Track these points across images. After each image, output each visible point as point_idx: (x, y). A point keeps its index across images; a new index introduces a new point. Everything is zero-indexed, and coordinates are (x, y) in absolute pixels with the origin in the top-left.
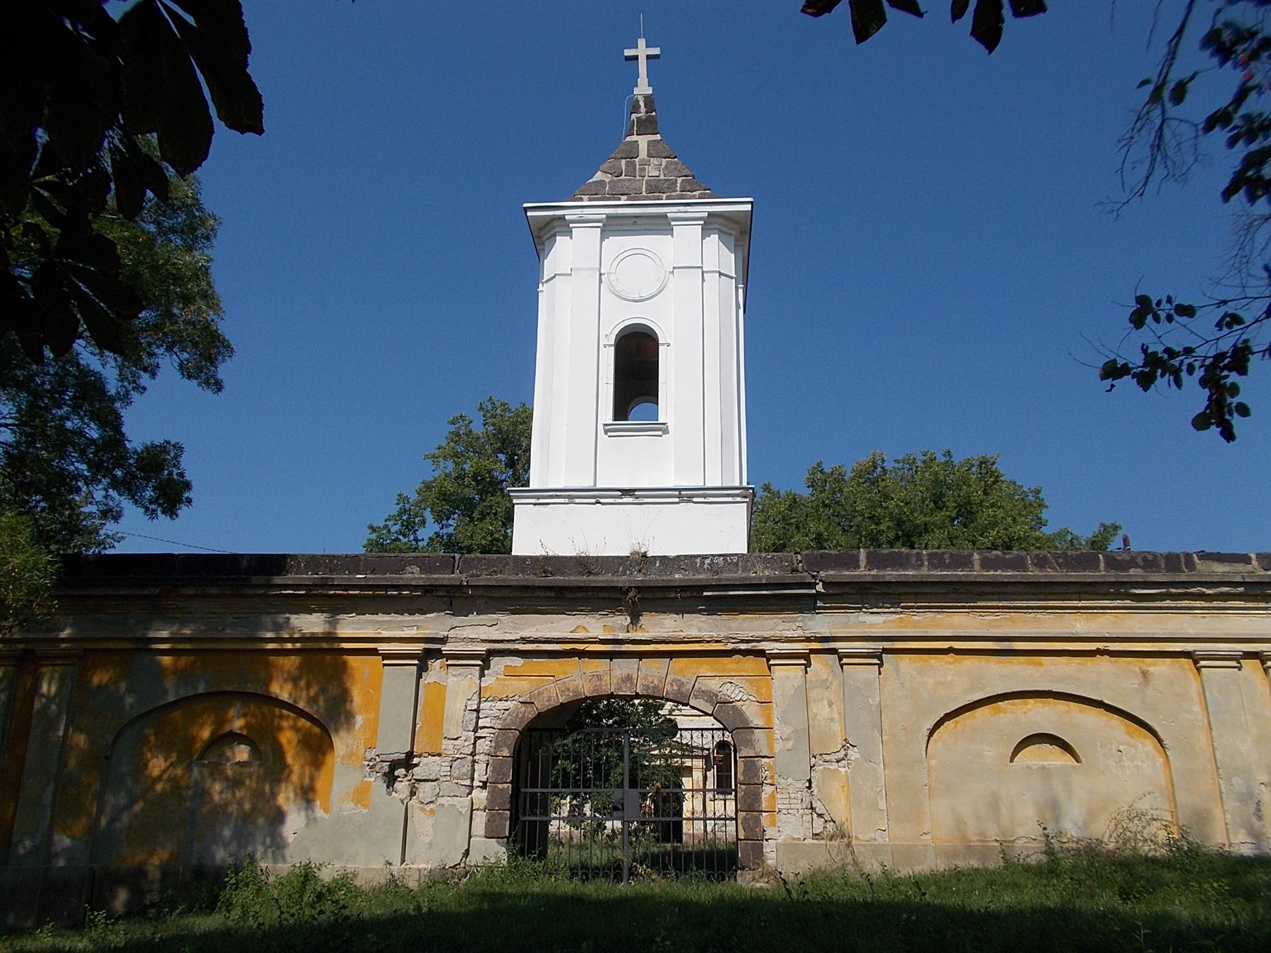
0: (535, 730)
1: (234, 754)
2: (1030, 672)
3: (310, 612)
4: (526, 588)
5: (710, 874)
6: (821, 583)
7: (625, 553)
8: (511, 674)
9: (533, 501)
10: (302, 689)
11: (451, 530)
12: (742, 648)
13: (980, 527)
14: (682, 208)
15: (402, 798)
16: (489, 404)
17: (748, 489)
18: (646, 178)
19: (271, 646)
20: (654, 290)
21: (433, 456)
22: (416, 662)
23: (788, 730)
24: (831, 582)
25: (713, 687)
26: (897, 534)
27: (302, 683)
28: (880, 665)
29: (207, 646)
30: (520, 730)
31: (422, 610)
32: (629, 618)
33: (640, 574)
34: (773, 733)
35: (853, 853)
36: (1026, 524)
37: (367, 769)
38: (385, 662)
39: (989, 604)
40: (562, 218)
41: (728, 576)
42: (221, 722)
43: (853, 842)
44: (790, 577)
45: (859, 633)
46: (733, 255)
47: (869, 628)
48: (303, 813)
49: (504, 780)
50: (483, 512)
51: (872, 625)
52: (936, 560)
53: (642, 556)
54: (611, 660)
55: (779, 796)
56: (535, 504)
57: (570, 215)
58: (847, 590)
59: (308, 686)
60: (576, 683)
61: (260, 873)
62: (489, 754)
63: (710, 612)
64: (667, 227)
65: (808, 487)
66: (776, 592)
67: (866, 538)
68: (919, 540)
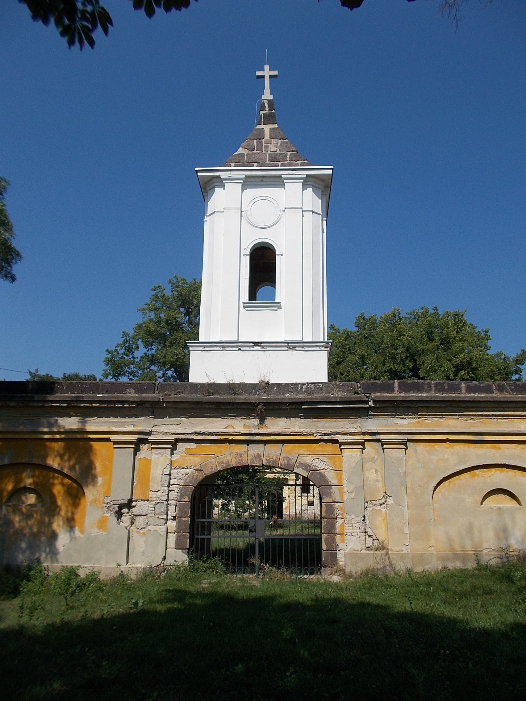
0: (204, 485)
1: (27, 499)
2: (493, 453)
3: (70, 416)
4: (198, 403)
5: (306, 569)
6: (372, 401)
7: (256, 381)
8: (189, 453)
9: (201, 349)
10: (65, 461)
11: (153, 352)
12: (325, 438)
13: (454, 352)
14: (291, 172)
15: (126, 526)
16: (175, 280)
17: (328, 343)
18: (269, 152)
19: (47, 436)
20: (273, 221)
21: (143, 310)
22: (133, 446)
23: (352, 487)
24: (378, 401)
25: (308, 461)
26: (407, 355)
27: (66, 458)
28: (406, 449)
29: (9, 436)
30: (195, 486)
31: (136, 415)
32: (258, 420)
33: (265, 395)
34: (343, 488)
35: (389, 558)
36: (481, 351)
37: (105, 509)
38: (115, 446)
39: (471, 413)
40: (219, 177)
41: (317, 396)
42: (19, 480)
43: (390, 552)
44: (353, 397)
45: (394, 430)
46: (321, 200)
47: (400, 427)
48: (68, 534)
49: (186, 516)
50: (171, 342)
51: (402, 426)
52: (440, 388)
53: (266, 384)
54: (248, 445)
55: (346, 525)
56: (202, 351)
57: (223, 175)
58: (387, 405)
59: (69, 459)
60: (227, 459)
61: (44, 569)
62: (176, 500)
63: (306, 417)
64: (281, 183)
65: (356, 327)
66: (345, 406)
67: (389, 357)
68: (419, 359)
